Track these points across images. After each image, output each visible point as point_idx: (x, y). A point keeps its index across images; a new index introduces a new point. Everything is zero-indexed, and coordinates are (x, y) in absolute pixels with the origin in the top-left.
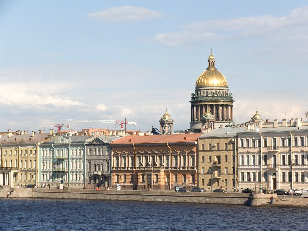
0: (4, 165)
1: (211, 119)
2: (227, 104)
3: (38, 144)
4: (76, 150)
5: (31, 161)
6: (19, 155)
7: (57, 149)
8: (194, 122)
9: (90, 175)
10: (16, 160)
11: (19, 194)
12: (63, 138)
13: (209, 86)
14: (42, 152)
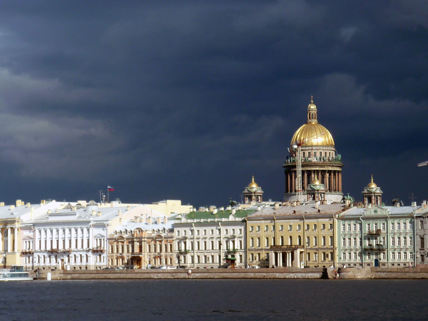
0: (279, 243)
1: (321, 189)
2: (335, 169)
3: (335, 217)
4: (349, 225)
5: (252, 239)
6: (305, 230)
7: (368, 222)
8: (292, 193)
9: (422, 253)
10: (299, 237)
11: (355, 275)
12: (376, 209)
13: (312, 146)
14: (342, 226)
